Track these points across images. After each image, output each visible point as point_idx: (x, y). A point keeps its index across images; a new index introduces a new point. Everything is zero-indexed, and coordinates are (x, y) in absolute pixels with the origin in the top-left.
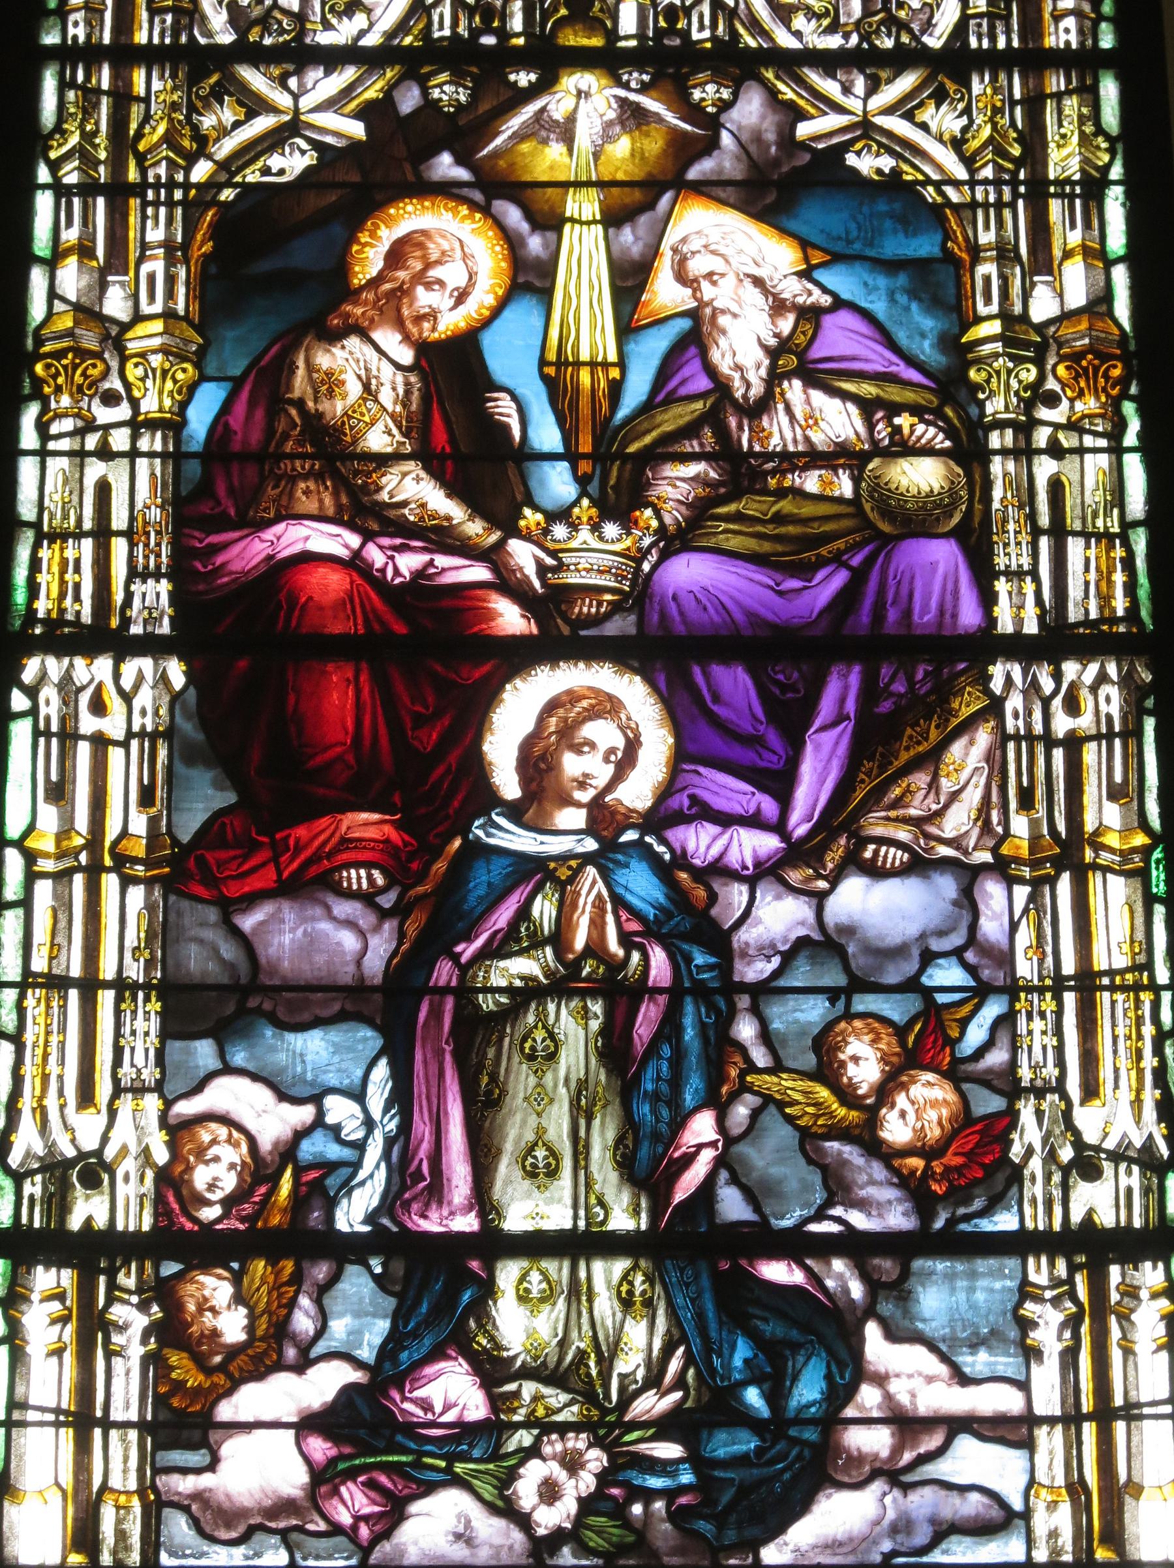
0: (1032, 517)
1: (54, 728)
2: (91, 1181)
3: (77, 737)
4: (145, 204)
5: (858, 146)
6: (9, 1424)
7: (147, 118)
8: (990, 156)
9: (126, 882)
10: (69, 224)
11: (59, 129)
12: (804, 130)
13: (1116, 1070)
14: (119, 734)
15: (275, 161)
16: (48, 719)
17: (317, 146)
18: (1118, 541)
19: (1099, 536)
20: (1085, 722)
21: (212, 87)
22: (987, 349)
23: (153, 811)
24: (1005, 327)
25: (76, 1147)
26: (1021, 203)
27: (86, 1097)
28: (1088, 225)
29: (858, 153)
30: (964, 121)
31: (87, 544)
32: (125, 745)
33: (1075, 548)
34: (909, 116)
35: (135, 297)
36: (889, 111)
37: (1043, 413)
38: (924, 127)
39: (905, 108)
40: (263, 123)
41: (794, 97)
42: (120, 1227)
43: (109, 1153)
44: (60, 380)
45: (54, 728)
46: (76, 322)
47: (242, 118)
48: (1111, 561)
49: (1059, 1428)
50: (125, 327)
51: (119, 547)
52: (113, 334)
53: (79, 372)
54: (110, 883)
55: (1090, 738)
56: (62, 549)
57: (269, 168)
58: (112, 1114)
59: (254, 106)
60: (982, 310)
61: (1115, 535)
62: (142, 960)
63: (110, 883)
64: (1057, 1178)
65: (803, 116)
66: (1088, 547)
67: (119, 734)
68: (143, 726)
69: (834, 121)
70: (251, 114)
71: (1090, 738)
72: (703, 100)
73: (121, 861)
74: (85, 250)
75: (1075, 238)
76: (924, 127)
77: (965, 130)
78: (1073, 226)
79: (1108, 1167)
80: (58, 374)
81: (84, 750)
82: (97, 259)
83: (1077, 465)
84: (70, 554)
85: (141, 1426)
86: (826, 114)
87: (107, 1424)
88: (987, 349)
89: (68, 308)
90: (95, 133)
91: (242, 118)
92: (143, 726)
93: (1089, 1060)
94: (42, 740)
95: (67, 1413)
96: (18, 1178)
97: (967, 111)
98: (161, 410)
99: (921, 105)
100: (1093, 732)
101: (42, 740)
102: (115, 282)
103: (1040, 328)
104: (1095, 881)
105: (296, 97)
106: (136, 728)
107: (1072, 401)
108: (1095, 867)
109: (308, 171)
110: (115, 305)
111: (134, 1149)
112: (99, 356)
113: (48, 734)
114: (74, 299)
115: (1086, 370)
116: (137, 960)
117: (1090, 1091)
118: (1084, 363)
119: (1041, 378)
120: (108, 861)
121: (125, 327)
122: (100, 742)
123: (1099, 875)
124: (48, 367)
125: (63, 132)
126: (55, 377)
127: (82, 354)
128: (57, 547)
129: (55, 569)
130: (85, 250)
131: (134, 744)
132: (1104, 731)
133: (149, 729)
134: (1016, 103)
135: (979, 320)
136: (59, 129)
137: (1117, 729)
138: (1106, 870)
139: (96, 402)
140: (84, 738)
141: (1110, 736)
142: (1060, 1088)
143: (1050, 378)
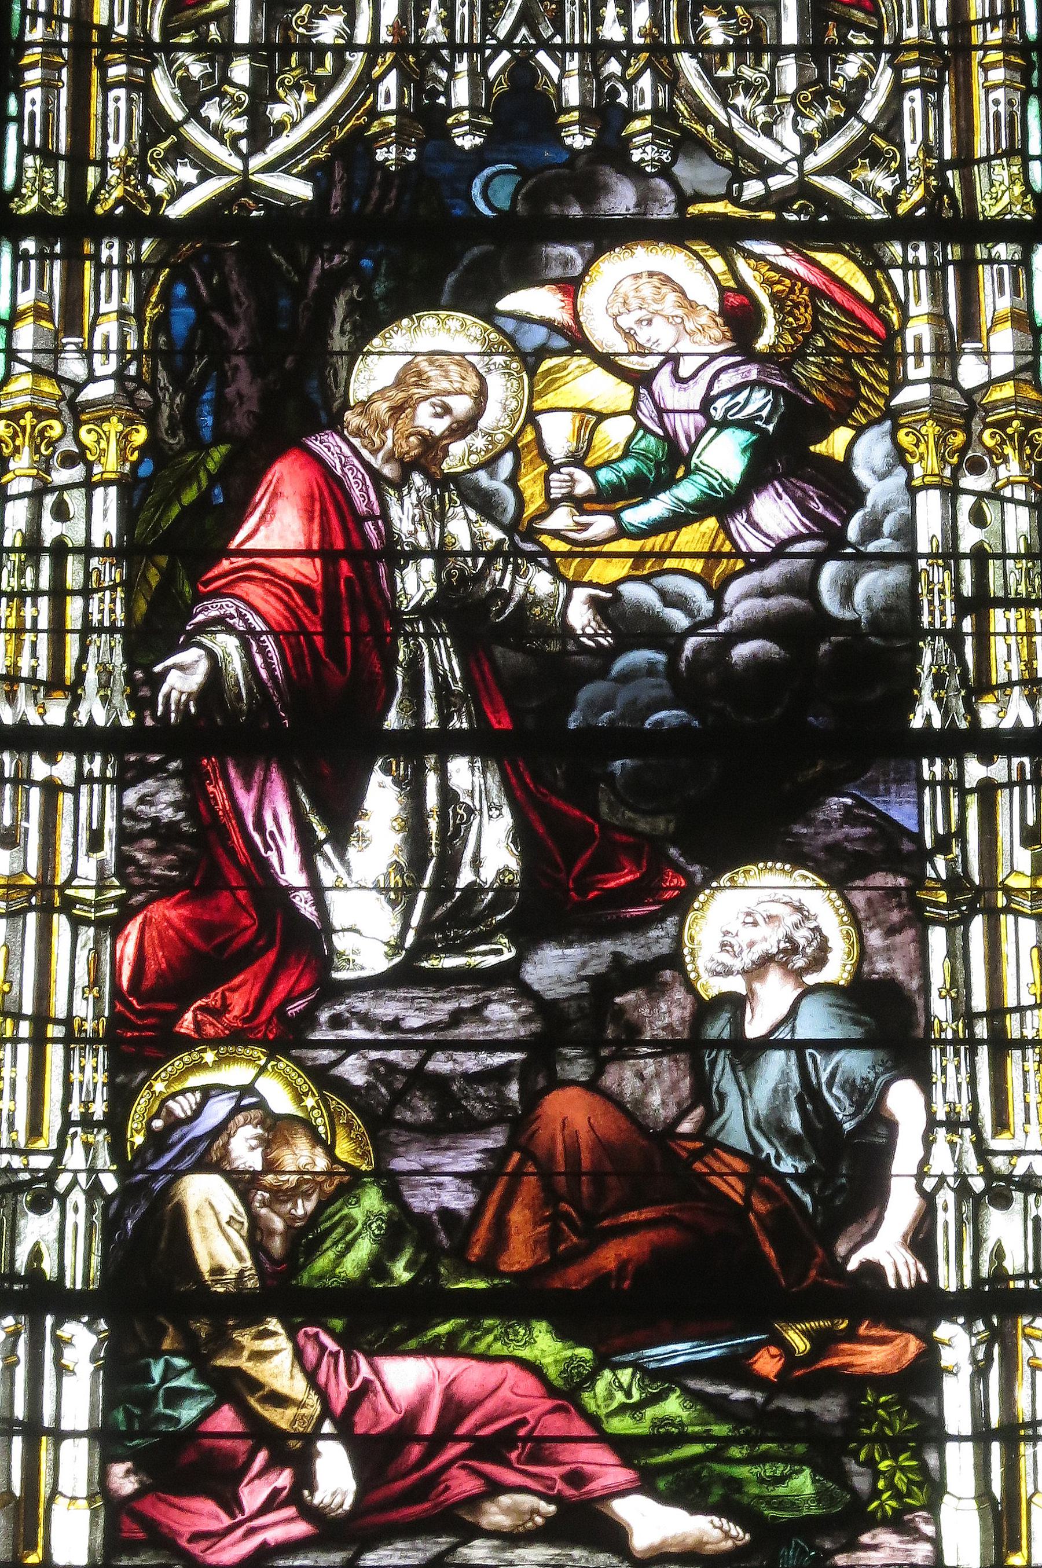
2: (40, 1206)
4: (99, 268)
7: (103, 182)
9: (76, 923)
10: (26, 286)
13: (1027, 1106)
14: (69, 781)
21: (167, 150)
23: (100, 855)
28: (1016, 292)
31: (44, 602)
32: (75, 791)
34: (845, 177)
36: (823, 171)
37: (968, 481)
51: (74, 607)
52: (68, 395)
54: (61, 924)
55: (1002, 786)
56: (19, 610)
60: (913, 374)
62: (91, 997)
63: (61, 924)
67: (69, 781)
70: (204, 177)
71: (1002, 786)
73: (68, 905)
74: (40, 313)
75: (1004, 304)
77: (897, 190)
78: (1002, 292)
79: (1018, 1196)
84: (28, 611)
85: (92, 1434)
87: (59, 1435)
89: (25, 369)
95: (1027, 1439)
97: (901, 170)
100: (1005, 780)
103: (968, 395)
104: (1007, 921)
108: (1007, 910)
110: (73, 367)
115: (1011, 437)
116: (87, 999)
117: (1001, 1123)
118: (1010, 431)
125: (22, 197)
130: (40, 313)
131: (84, 789)
132: (1015, 777)
135: (907, 382)
137: (1028, 777)
138: (1017, 914)
142: (974, 1123)
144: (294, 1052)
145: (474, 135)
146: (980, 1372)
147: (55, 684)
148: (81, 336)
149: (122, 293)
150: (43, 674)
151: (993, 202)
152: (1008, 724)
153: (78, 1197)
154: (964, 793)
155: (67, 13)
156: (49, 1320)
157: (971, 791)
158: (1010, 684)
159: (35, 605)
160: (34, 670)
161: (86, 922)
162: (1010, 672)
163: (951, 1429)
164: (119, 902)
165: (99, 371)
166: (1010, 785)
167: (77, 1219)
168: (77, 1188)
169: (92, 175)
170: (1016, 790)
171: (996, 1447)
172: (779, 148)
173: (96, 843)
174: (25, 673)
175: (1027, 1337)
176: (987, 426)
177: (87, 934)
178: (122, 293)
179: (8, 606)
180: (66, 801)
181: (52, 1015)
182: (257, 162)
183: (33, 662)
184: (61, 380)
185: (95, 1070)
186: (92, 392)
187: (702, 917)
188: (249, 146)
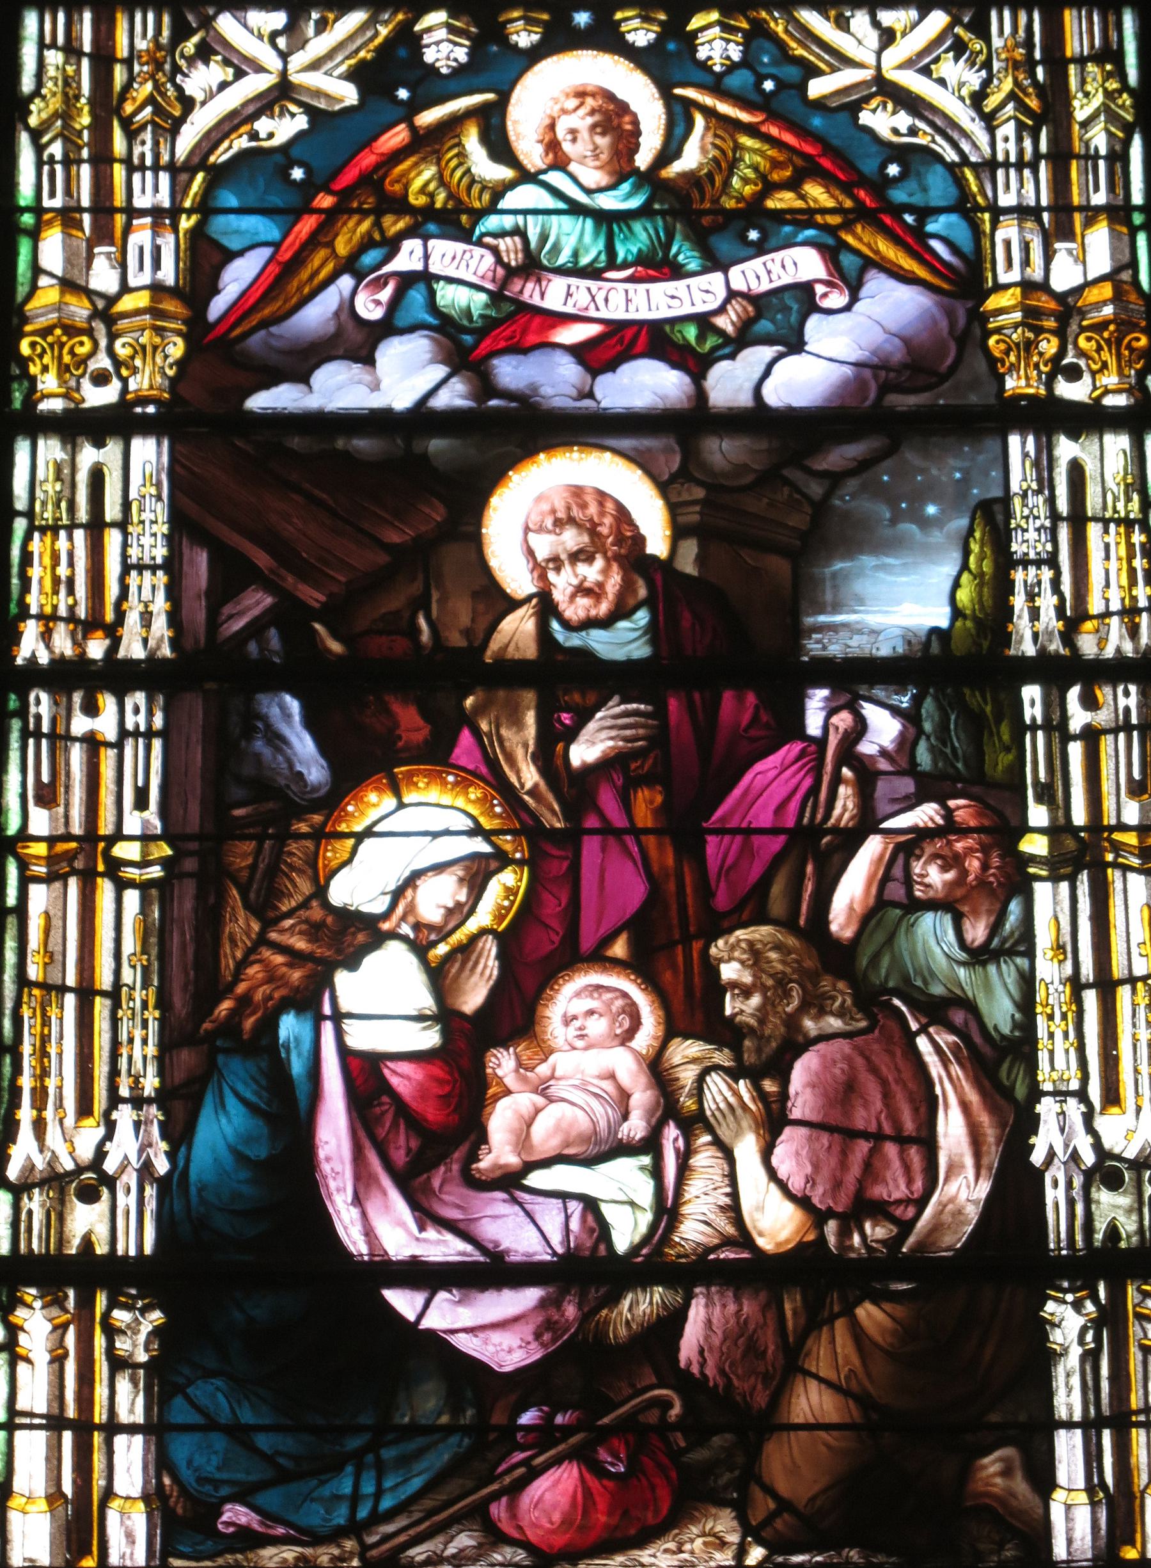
0: (1051, 501)
1: (45, 728)
2: (89, 1195)
3: (69, 738)
4: (131, 169)
5: (874, 103)
6: (10, 1427)
7: (131, 79)
8: (1012, 113)
9: (121, 885)
11: (37, 93)
12: (817, 88)
15: (263, 125)
16: (38, 717)
17: (310, 110)
18: (1137, 527)
19: (1118, 522)
20: (1103, 718)
22: (1003, 320)
23: (146, 814)
24: (1025, 295)
25: (74, 1159)
26: (1043, 165)
27: (84, 1109)
29: (874, 111)
30: (984, 73)
32: (119, 745)
33: (1093, 531)
34: (926, 71)
35: (123, 266)
38: (942, 82)
39: (922, 62)
40: (255, 84)
41: (806, 54)
42: (120, 1251)
43: (110, 1166)
44: (47, 359)
45: (45, 728)
46: (62, 293)
47: (230, 78)
48: (1130, 546)
49: (1078, 1432)
50: (112, 300)
53: (66, 350)
54: (105, 890)
55: (1106, 732)
57: (257, 133)
58: (111, 1127)
59: (241, 66)
61: (1135, 521)
64: (1078, 1181)
65: (817, 72)
66: (1106, 531)
67: (111, 735)
68: (137, 725)
69: (847, 77)
70: (240, 74)
71: (1106, 732)
72: (710, 58)
76: (942, 82)
80: (44, 351)
81: (77, 754)
82: (83, 230)
83: (1096, 447)
84: (62, 544)
86: (839, 70)
87: (113, 1428)
88: (1003, 320)
89: (54, 281)
90: (77, 97)
91: (230, 78)
92: (137, 725)
93: (1110, 1062)
94: (31, 741)
96: (19, 1190)
97: (987, 65)
98: (151, 387)
99: (937, 60)
101: (31, 741)
102: (100, 253)
103: (1061, 298)
105: (284, 56)
106: (130, 726)
107: (1094, 374)
109: (300, 136)
110: (104, 278)
111: (135, 1163)
112: (90, 332)
113: (38, 735)
114: (59, 273)
117: (1112, 1097)
119: (1062, 352)
120: (101, 868)
121: (112, 300)
122: (92, 742)
123: (1118, 874)
124: (33, 345)
126: (41, 356)
127: (71, 330)
128: (48, 539)
129: (47, 561)
130: (68, 217)
133: (142, 728)
134: (1038, 63)
135: (999, 288)
136: (37, 93)
138: (1126, 869)
139: (86, 383)
140: (76, 739)
141: (1128, 728)
142: (1082, 1095)
143: (1071, 352)
144: (322, 882)
145: (530, 32)
146: (1091, 1357)
147: (92, 624)
148: (112, 244)
149: (156, 189)
150: (81, 611)
151: (1085, 101)
152: (1109, 652)
153: (130, 1178)
154: (1067, 738)
155: (87, 48)
156: (101, 1301)
157: (1075, 738)
158: (1107, 614)
159: (70, 538)
160: (71, 609)
161: (131, 884)
162: (1107, 600)
163: (1062, 1413)
164: (165, 862)
165: (133, 282)
166: (1115, 731)
167: (126, 1201)
168: (129, 1169)
169: (119, 75)
170: (1122, 736)
171: (1107, 1435)
172: (856, 43)
173: (141, 803)
174: (63, 612)
175: (1140, 1317)
176: (1083, 329)
177: (132, 897)
178: (156, 189)
179: (42, 540)
180: (108, 759)
181: (97, 986)
182: (298, 60)
183: (70, 601)
184: (89, 293)
185: (145, 1042)
186: (127, 303)
187: (556, 101)
188: (288, 45)
